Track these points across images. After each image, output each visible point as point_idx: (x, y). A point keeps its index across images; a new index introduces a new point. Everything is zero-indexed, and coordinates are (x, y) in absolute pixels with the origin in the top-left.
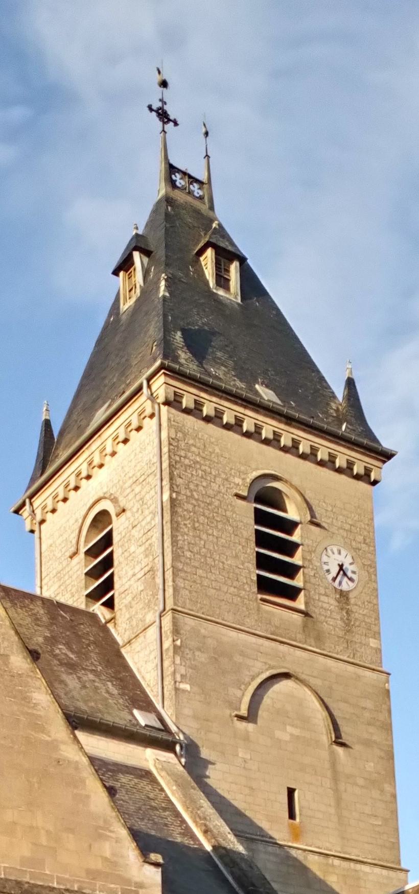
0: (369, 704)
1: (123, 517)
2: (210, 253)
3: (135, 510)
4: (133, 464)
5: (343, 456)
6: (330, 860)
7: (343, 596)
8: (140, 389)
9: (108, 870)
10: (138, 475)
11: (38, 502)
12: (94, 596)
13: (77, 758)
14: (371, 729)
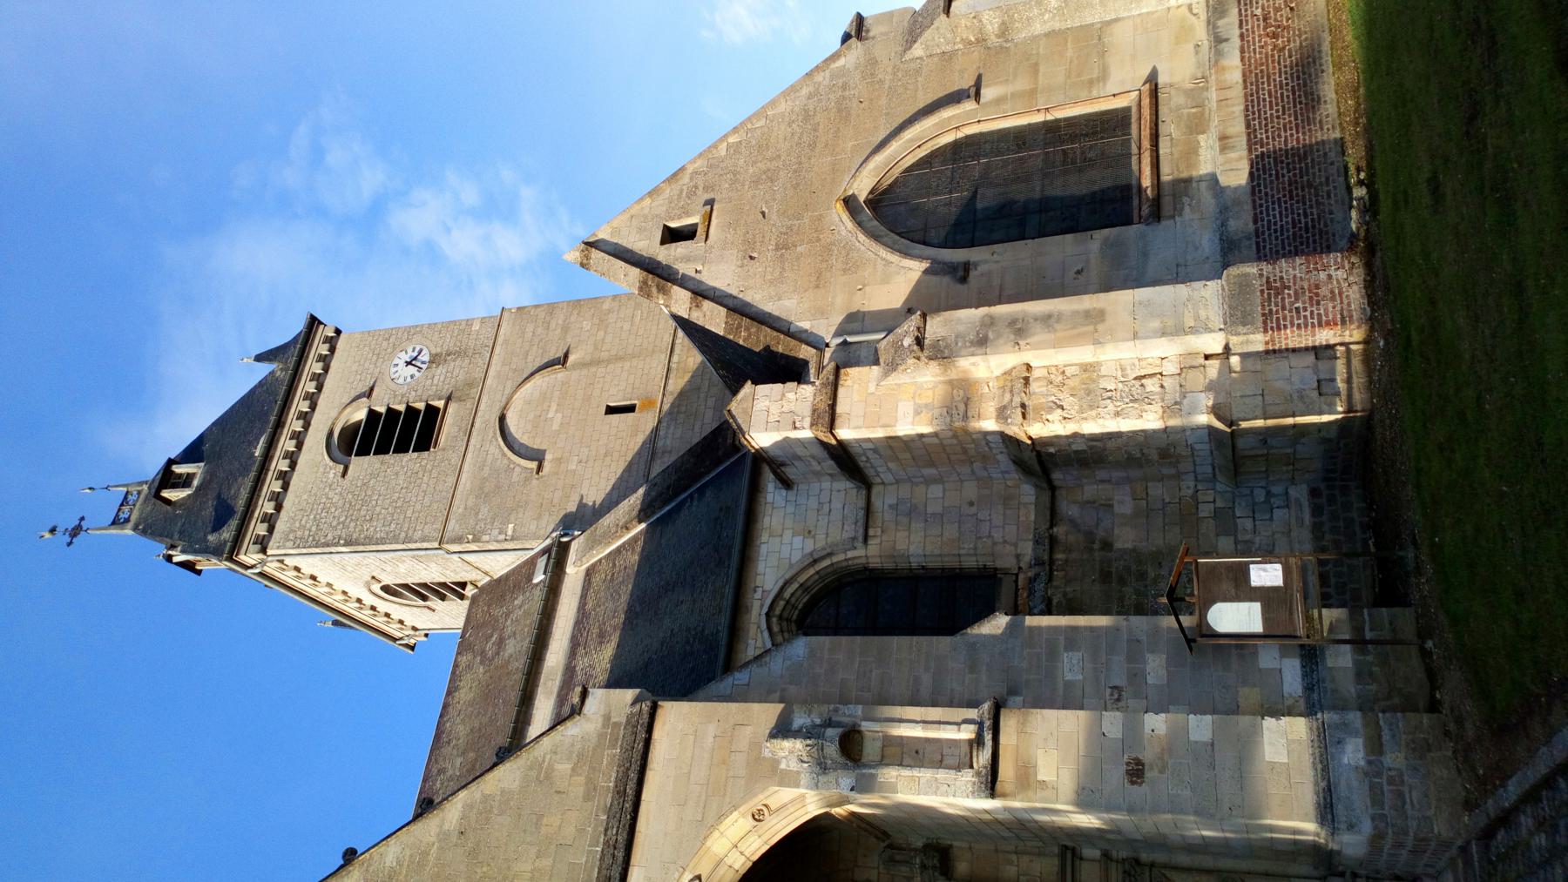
0: (530, 328)
5: (313, 366)
6: (673, 366)
7: (435, 360)
8: (261, 574)
9: (586, 768)
11: (398, 634)
12: (462, 597)
13: (459, 806)
14: (553, 325)
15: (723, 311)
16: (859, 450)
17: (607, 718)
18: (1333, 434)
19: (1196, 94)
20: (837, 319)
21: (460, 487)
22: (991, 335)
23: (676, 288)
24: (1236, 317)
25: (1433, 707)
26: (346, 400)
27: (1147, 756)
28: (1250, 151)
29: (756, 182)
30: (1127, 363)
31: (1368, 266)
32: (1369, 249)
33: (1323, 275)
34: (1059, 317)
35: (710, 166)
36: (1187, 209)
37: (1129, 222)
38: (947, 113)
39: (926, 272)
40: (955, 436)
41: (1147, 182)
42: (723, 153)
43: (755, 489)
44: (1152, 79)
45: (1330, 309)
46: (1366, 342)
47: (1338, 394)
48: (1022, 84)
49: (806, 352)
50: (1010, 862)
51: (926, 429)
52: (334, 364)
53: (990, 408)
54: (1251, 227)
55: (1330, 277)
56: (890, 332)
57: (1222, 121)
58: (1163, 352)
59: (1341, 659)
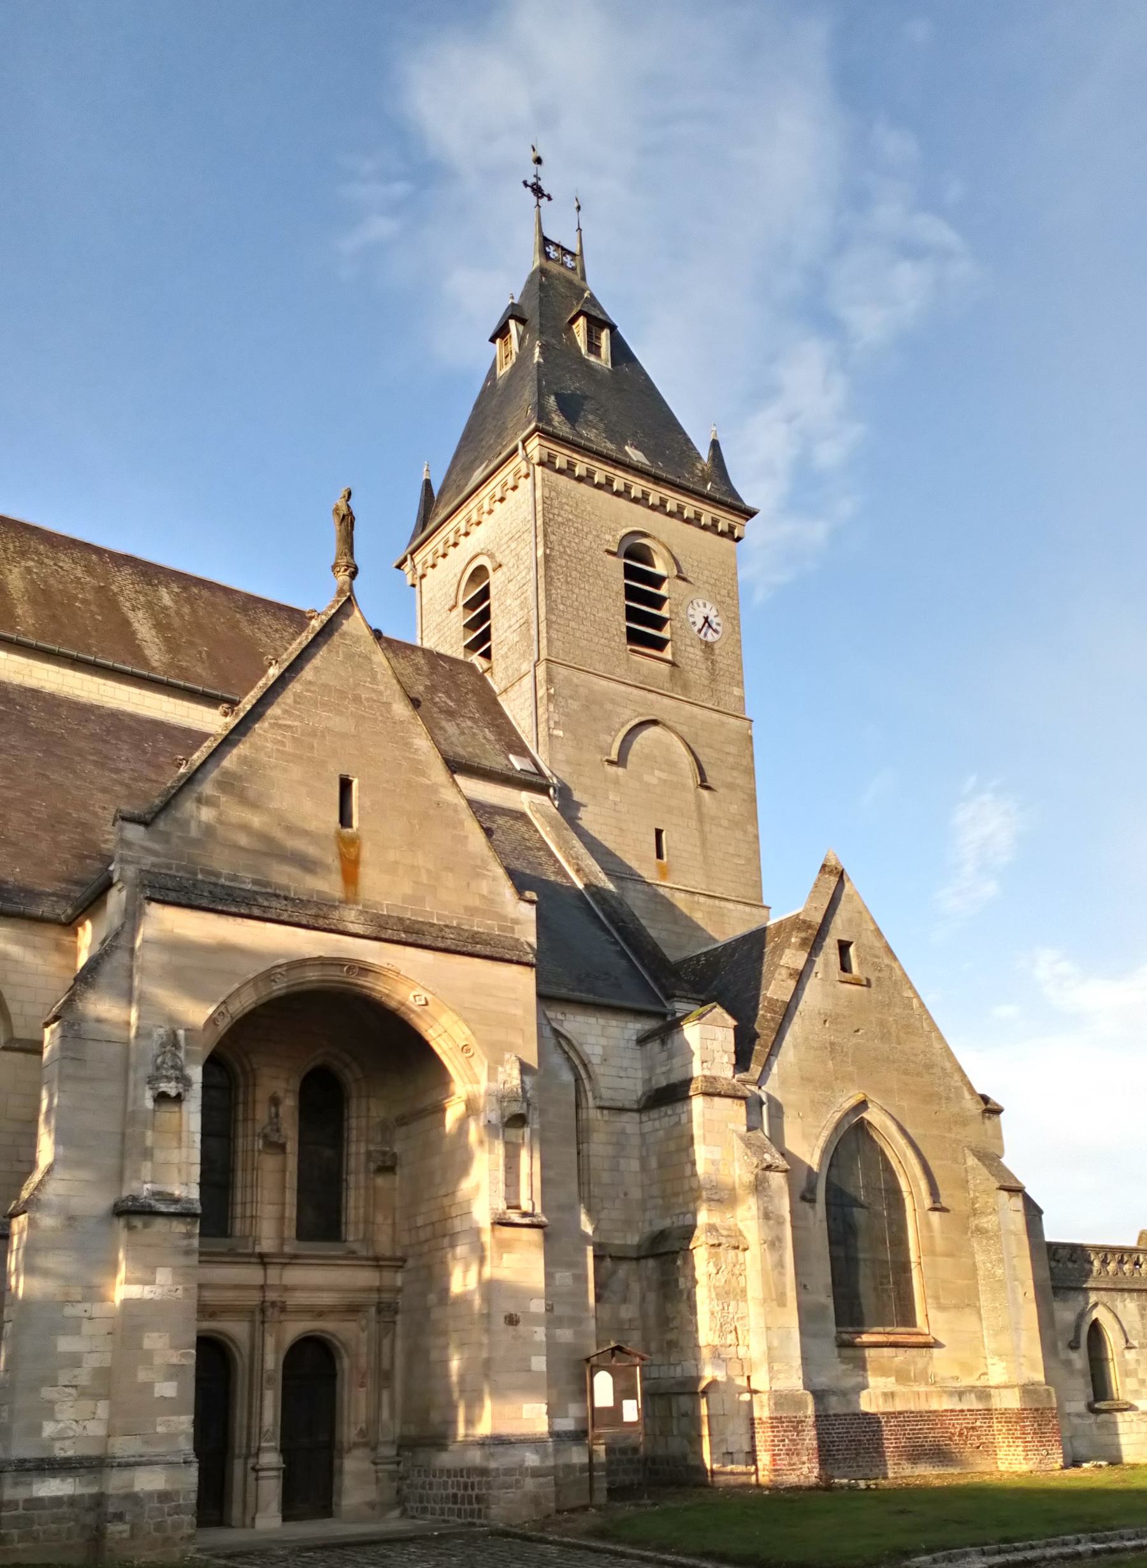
0: (732, 749)
1: (499, 572)
2: (582, 321)
3: (511, 565)
4: (509, 521)
5: (708, 513)
6: (696, 898)
7: (709, 647)
8: (515, 450)
9: (485, 907)
10: (514, 532)
11: (418, 557)
12: (472, 647)
14: (735, 773)
15: (787, 999)
16: (679, 1110)
17: (516, 922)
18: (692, 1461)
19: (923, 1376)
20: (778, 1096)
21: (595, 679)
22: (772, 1222)
23: (806, 955)
24: (781, 1399)
25: (559, 1512)
26: (676, 551)
27: (102, 1202)
28: (883, 1413)
29: (882, 1024)
30: (747, 1322)
31: (810, 1488)
32: (825, 1487)
33: (805, 1458)
34: (782, 1274)
35: (896, 983)
36: (844, 1367)
37: (838, 1324)
38: (923, 1185)
39: (810, 1169)
40: (692, 1189)
41: (865, 1338)
42: (905, 994)
43: (638, 1013)
44: (937, 1344)
45: (783, 1462)
46: (758, 1485)
47: (724, 1466)
48: (940, 1244)
49: (755, 1069)
50: (386, 1218)
51: (700, 1168)
52: (708, 535)
53: (716, 1219)
54: (831, 1412)
55: (804, 1463)
56: (770, 1139)
57: (904, 1394)
58: (754, 1347)
59: (577, 1456)
